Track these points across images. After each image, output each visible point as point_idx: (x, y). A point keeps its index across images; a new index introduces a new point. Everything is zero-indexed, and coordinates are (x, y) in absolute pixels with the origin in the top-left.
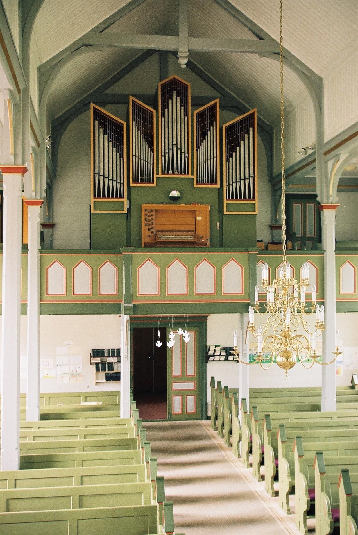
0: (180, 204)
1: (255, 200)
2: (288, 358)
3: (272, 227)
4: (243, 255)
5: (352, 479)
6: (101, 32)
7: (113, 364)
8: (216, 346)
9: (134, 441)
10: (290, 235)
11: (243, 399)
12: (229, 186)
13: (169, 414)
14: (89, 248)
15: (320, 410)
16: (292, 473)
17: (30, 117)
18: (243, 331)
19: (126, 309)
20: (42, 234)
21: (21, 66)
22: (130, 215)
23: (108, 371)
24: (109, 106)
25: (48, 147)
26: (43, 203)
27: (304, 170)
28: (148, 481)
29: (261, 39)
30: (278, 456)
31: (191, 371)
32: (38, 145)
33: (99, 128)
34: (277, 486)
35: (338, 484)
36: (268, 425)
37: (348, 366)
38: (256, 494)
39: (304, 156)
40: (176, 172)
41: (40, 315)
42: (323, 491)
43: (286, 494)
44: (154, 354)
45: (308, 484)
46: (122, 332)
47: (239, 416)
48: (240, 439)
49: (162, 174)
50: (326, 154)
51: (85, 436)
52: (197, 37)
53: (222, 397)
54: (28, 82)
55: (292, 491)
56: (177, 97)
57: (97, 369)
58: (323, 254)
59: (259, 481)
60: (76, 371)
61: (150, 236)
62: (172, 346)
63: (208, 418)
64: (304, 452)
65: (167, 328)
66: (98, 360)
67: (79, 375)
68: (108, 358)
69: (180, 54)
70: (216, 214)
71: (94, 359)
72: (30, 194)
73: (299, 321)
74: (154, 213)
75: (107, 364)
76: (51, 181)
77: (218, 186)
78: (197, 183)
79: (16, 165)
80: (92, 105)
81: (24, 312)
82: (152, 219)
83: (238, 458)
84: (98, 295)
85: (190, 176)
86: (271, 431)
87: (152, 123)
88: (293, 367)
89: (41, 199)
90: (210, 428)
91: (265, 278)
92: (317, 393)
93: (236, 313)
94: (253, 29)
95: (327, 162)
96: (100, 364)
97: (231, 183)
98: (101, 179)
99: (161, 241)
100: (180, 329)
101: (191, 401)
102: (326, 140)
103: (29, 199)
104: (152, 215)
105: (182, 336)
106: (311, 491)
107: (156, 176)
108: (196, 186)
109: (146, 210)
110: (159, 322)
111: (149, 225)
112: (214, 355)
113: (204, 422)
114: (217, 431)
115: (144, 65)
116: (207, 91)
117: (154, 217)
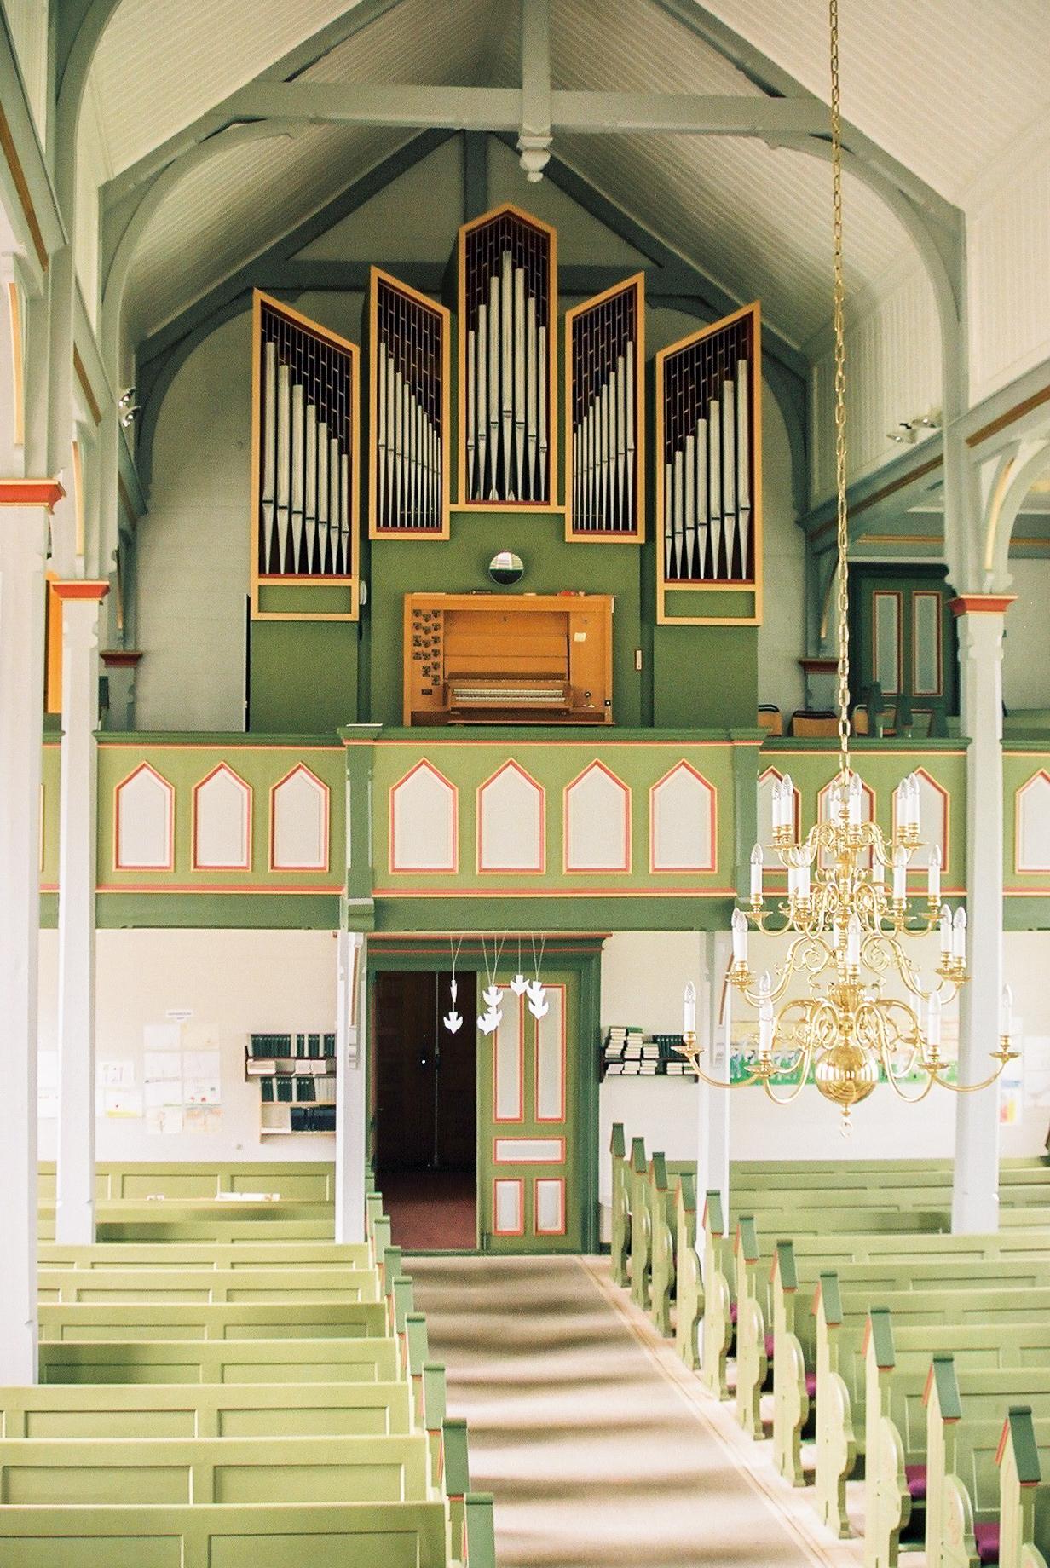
1: (754, 583)
2: (850, 1069)
4: (715, 752)
6: (289, 80)
9: (375, 1311)
13: (482, 1234)
15: (947, 1230)
16: (857, 1418)
17: (73, 333)
19: (355, 914)
20: (103, 681)
22: (369, 628)
24: (308, 299)
25: (126, 424)
26: (107, 590)
28: (417, 1433)
29: (773, 93)
30: (814, 1367)
31: (552, 1103)
32: (97, 417)
33: (277, 365)
34: (810, 1454)
35: (998, 1451)
37: (1035, 1096)
38: (746, 1477)
39: (906, 447)
40: (510, 497)
42: (952, 1472)
44: (437, 1052)
45: (905, 1448)
46: (341, 984)
47: (696, 1245)
48: (701, 1313)
49: (468, 502)
50: (974, 441)
51: (230, 1294)
52: (578, 89)
53: (646, 1186)
55: (857, 1469)
56: (514, 267)
57: (267, 1095)
58: (964, 749)
59: (755, 1439)
60: (204, 1099)
61: (429, 692)
63: (603, 1249)
65: (478, 974)
66: (268, 1067)
67: (213, 1109)
68: (299, 1062)
69: (524, 142)
70: (633, 624)
71: (257, 1063)
72: (71, 566)
73: (887, 957)
74: (440, 620)
75: (294, 1081)
76: (134, 526)
77: (640, 538)
78: (575, 530)
80: (259, 296)
81: (48, 917)
82: (436, 640)
83: (694, 1369)
84: (270, 870)
85: (554, 508)
86: (797, 1292)
87: (437, 348)
88: (868, 1092)
90: (607, 1280)
93: (691, 929)
94: (748, 65)
95: (977, 465)
96: (274, 1081)
97: (679, 528)
101: (550, 1196)
102: (974, 399)
104: (436, 627)
105: (525, 999)
106: (915, 1472)
107: (448, 508)
108: (570, 537)
109: (417, 613)
110: (455, 954)
111: (427, 657)
112: (622, 1059)
113: (591, 1260)
116: (606, 249)
117: (440, 633)
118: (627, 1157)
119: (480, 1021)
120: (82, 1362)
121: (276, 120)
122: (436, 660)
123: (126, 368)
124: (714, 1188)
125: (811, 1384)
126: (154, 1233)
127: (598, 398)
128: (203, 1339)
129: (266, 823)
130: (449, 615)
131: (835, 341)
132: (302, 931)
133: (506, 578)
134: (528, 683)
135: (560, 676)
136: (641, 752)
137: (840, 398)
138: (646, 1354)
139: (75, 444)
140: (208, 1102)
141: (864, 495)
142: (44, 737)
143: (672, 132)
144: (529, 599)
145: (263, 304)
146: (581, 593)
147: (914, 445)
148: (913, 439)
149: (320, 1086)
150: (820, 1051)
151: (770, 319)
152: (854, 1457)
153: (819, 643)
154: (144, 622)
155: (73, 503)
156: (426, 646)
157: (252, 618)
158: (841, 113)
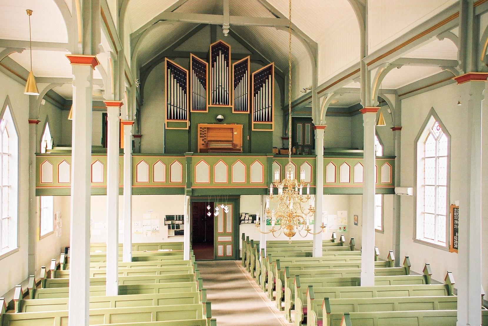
0: (223, 124)
1: (272, 122)
2: (291, 230)
3: (283, 138)
4: (264, 158)
5: (330, 303)
6: (172, 12)
7: (179, 225)
8: (246, 214)
9: (192, 276)
10: (294, 144)
11: (262, 249)
12: (255, 112)
13: (215, 256)
14: (164, 152)
15: (312, 256)
16: (293, 297)
17: (124, 67)
18: (263, 206)
19: (188, 192)
20: (133, 142)
21: (118, 36)
22: (191, 131)
23: (176, 229)
24: (178, 59)
25: (137, 87)
26: (134, 123)
27: (305, 102)
28: (200, 303)
29: (278, 17)
30: (284, 286)
31: (229, 229)
32: (131, 86)
33: (171, 74)
34: (283, 304)
35: (322, 305)
36: (278, 265)
37: (330, 227)
38: (270, 309)
39: (304, 94)
40: (221, 104)
41: (132, 195)
42: (312, 310)
43: (289, 310)
44: (206, 218)
45: (302, 304)
46: (185, 206)
47: (260, 259)
48: (260, 274)
49: (212, 105)
50: (319, 93)
51: (161, 273)
52: (236, 15)
53: (249, 246)
54: (123, 45)
55: (293, 308)
56: (222, 54)
57: (169, 228)
58: (316, 157)
59: (272, 301)
60: (155, 229)
61: (204, 144)
62: (217, 215)
63: (240, 259)
64: (300, 284)
65: (214, 202)
66: (170, 222)
67: (158, 231)
68: (176, 221)
69: (224, 27)
70: (247, 131)
71: (167, 222)
72: (125, 117)
73: (298, 207)
74: (206, 130)
75: (175, 225)
76: (140, 108)
77: (249, 112)
78: (235, 111)
79: (116, 101)
80: (166, 59)
81: (121, 192)
82: (205, 134)
83: (259, 285)
84: (170, 182)
85: (230, 106)
86: (280, 271)
87: (205, 71)
88: (294, 235)
89: (132, 120)
90: (241, 266)
91: (277, 179)
92: (309, 244)
93: (258, 195)
94: (272, 11)
95: (319, 98)
96: (171, 225)
97: (257, 110)
98: (172, 107)
99: (210, 147)
100: (223, 205)
101: (229, 249)
102: (319, 85)
103: (124, 121)
104: (205, 131)
105: (224, 209)
106: (305, 309)
107: (208, 106)
108: (233, 112)
109: (201, 128)
110: (209, 198)
111: (203, 137)
112: (244, 220)
113: (238, 261)
114: (246, 268)
115: (199, 34)
116: (242, 50)
117: (206, 132)
118: (246, 240)
119: (214, 214)
120: (128, 289)
121: (171, 21)
122: (205, 135)
123: (137, 75)
124: (263, 248)
125: (284, 290)
126: (145, 259)
127: (239, 83)
128: (155, 283)
129: (169, 175)
130: (208, 128)
131: (289, 78)
132: (177, 195)
133: (220, 121)
134: (225, 142)
135: (231, 141)
136: (248, 158)
137: (290, 90)
138: (250, 282)
139: (126, 91)
140: (156, 230)
141: (295, 104)
142: (120, 154)
143: (257, 26)
144: (225, 125)
145: (167, 61)
146: (236, 124)
147: (305, 94)
148: (306, 92)
149: (181, 226)
150: (284, 226)
151: (277, 66)
152: (292, 305)
153: (286, 134)
154: (142, 129)
155: (125, 107)
156: (203, 137)
157: (166, 129)
158: (291, 21)
